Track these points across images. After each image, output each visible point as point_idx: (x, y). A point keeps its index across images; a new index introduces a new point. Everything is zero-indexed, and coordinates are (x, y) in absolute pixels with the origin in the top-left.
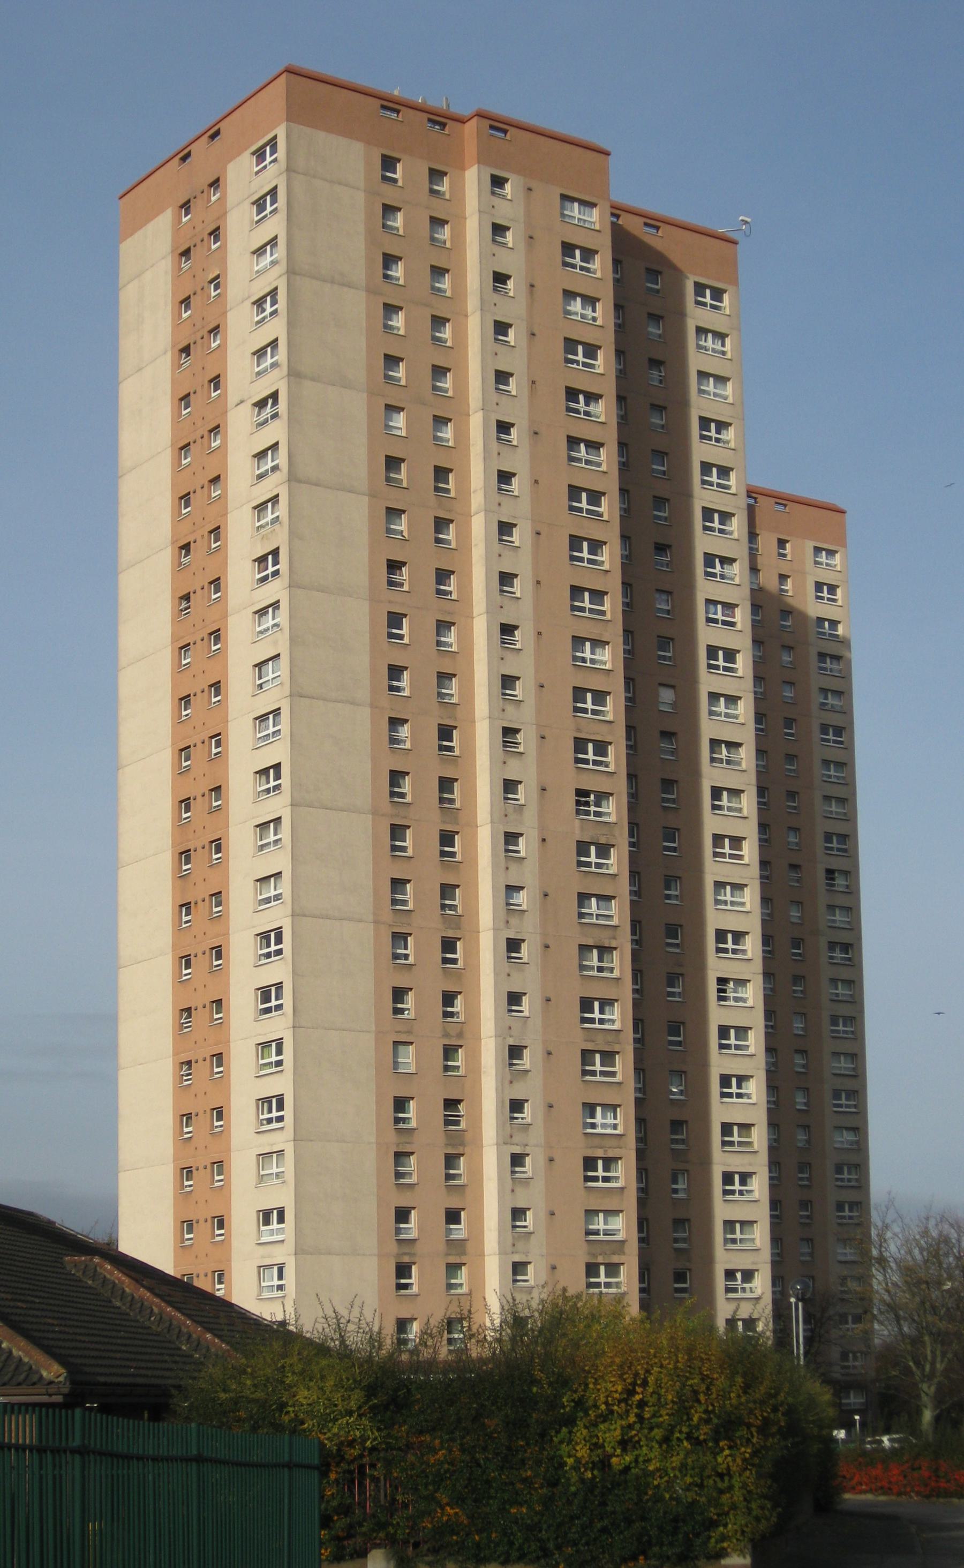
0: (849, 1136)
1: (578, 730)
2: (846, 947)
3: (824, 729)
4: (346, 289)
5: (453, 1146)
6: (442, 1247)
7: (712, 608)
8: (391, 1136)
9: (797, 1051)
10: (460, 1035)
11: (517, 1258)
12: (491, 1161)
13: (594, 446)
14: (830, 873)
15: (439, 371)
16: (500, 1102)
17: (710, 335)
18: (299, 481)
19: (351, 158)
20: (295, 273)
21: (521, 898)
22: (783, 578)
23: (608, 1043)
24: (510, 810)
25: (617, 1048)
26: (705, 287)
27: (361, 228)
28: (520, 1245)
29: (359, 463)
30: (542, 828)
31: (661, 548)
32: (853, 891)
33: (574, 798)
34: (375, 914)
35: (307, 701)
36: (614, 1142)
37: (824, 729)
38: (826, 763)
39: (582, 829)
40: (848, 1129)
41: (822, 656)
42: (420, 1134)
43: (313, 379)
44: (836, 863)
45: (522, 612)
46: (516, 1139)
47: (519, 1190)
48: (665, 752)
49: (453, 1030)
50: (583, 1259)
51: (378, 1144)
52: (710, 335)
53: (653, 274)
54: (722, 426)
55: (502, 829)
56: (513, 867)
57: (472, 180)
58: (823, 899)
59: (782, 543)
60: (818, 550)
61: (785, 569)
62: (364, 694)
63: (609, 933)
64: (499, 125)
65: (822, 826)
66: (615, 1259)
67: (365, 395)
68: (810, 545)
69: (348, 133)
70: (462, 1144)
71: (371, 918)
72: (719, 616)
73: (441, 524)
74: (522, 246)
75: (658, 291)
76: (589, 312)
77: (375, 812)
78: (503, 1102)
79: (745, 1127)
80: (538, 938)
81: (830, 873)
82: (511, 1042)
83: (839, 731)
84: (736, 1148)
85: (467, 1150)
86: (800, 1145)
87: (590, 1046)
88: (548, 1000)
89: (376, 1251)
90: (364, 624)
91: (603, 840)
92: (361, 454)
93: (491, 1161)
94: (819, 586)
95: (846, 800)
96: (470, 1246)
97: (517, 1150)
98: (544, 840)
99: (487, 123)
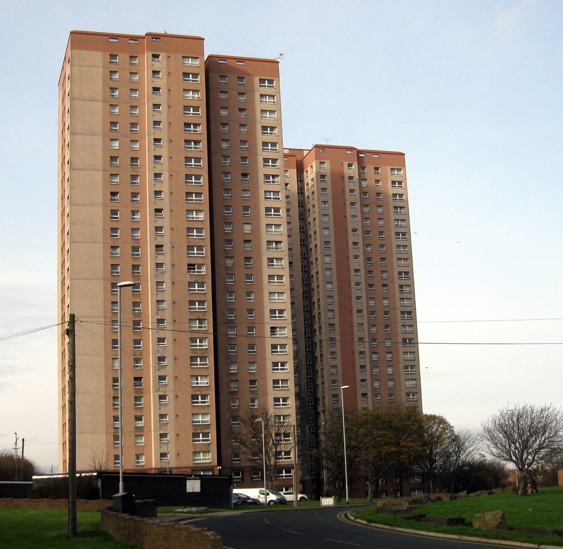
0: (414, 382)
1: (189, 243)
2: (409, 313)
3: (397, 234)
4: (94, 102)
5: (138, 393)
6: (133, 429)
7: (268, 194)
8: (111, 391)
9: (387, 353)
10: (141, 354)
11: (161, 432)
12: (152, 398)
13: (197, 142)
14: (401, 286)
15: (134, 125)
16: (154, 377)
17: (267, 97)
18: (74, 169)
19: (97, 58)
20: (73, 100)
21: (165, 305)
22: (377, 181)
23: (202, 353)
24: (159, 274)
25: (206, 355)
26: (264, 80)
27: (101, 80)
28: (163, 428)
29: (98, 158)
30: (172, 278)
31: (245, 175)
32: (412, 292)
33: (187, 267)
34: (104, 315)
35: (76, 244)
36: (205, 389)
37: (397, 234)
38: (398, 246)
39: (190, 278)
40: (411, 380)
41: (396, 208)
42: (127, 390)
43: (80, 134)
44: (403, 283)
45: (165, 202)
46: (160, 390)
47: (162, 408)
48: (248, 247)
49: (138, 353)
50: (191, 431)
51: (105, 394)
52: (267, 97)
53: (241, 78)
54: (272, 128)
55: (155, 281)
56: (160, 294)
57: (147, 56)
58: (398, 296)
59: (376, 169)
60: (391, 169)
61: (378, 178)
62: (100, 239)
63: (202, 314)
64: (155, 37)
65: (396, 270)
66: (206, 431)
67: (101, 137)
68: (389, 168)
69: (97, 49)
70: (142, 393)
71: (103, 316)
72: (272, 196)
73: (134, 177)
74: (165, 77)
75: (244, 84)
76: (196, 96)
77: (104, 279)
78: (155, 377)
79: (285, 381)
80: (171, 318)
81: (401, 286)
82: (159, 355)
83: (404, 234)
84: (280, 389)
85: (144, 395)
86: (390, 387)
87: (194, 355)
88: (175, 340)
89: (105, 432)
90: (101, 216)
91: (200, 281)
92: (100, 156)
93: (152, 398)
94: (394, 182)
95: (408, 258)
96: (145, 429)
97: (162, 394)
98: (173, 283)
99: (151, 37)
